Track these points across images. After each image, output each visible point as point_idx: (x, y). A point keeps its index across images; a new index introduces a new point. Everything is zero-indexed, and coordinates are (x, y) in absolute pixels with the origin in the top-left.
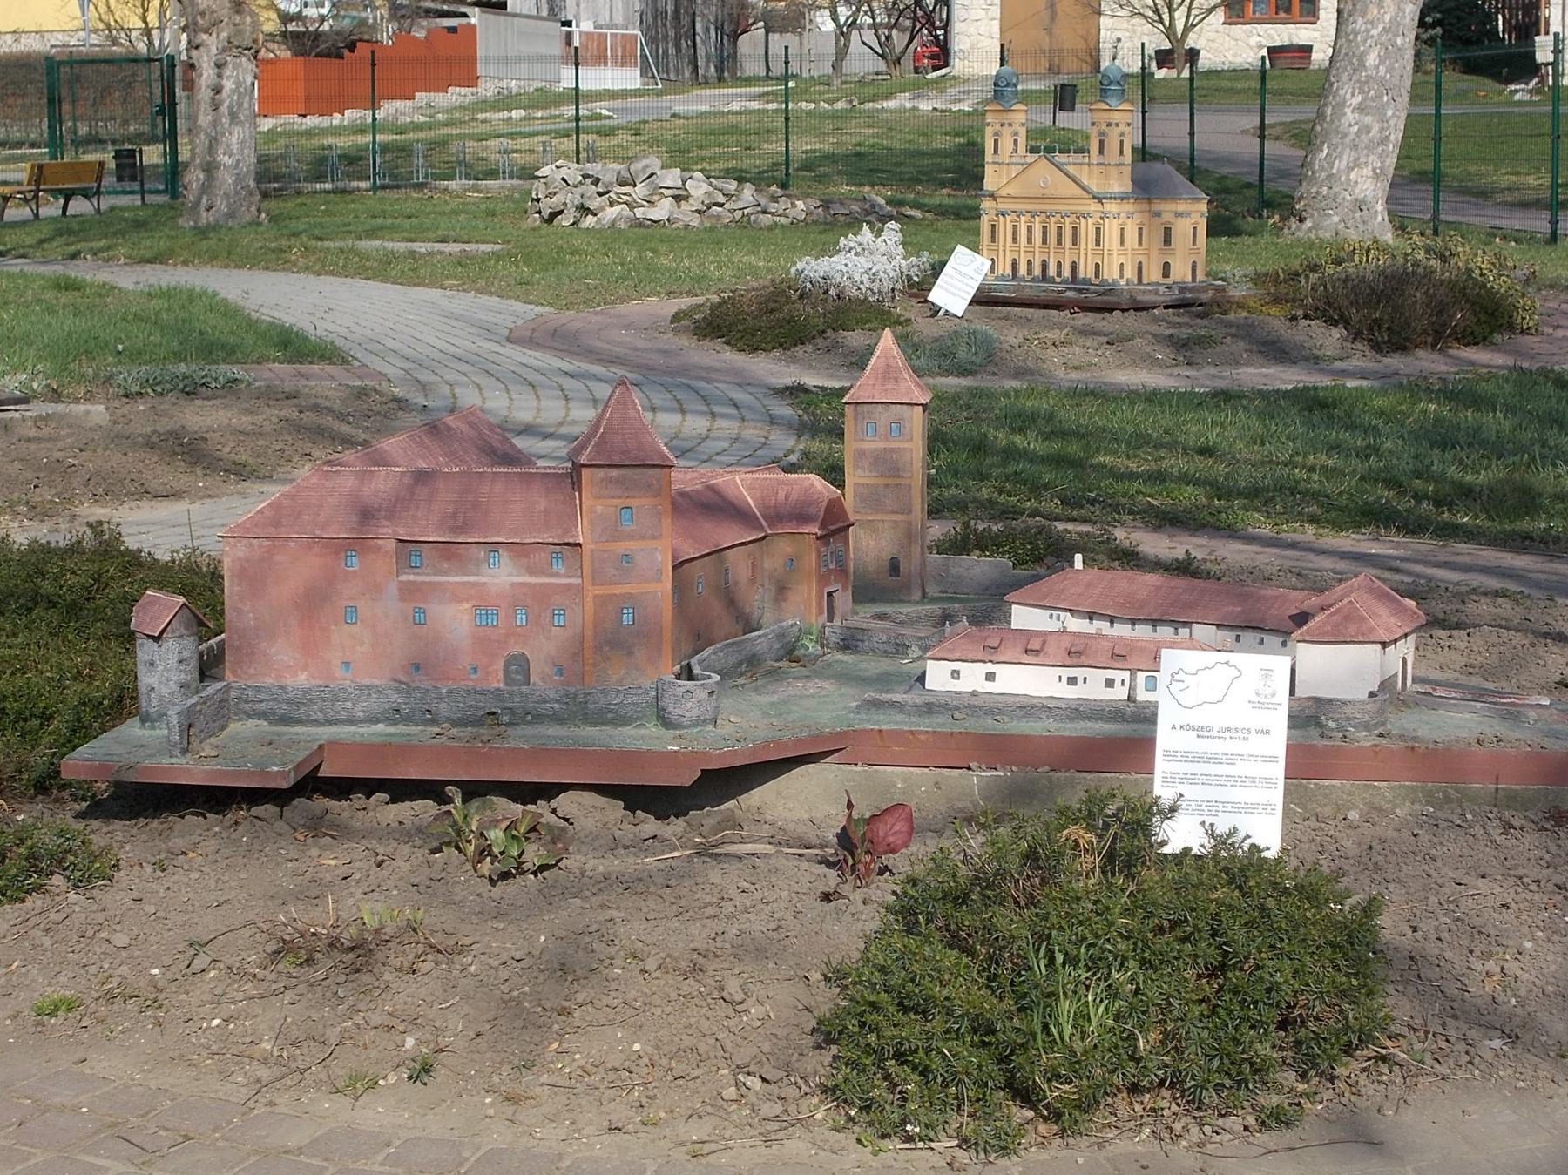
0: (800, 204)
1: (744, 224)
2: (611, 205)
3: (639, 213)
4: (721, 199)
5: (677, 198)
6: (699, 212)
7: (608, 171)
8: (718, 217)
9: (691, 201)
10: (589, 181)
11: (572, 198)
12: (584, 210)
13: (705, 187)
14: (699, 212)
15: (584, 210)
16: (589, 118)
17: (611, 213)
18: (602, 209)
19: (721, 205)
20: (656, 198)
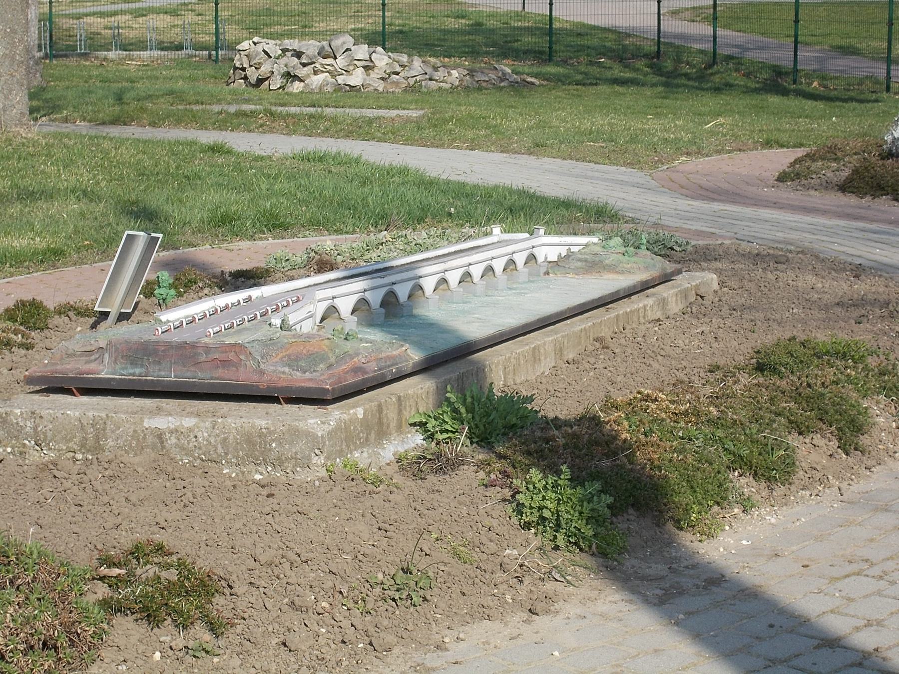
0: (455, 73)
1: (413, 89)
2: (316, 73)
3: (340, 80)
4: (398, 69)
5: (367, 68)
6: (382, 79)
7: (310, 47)
8: (397, 84)
9: (376, 70)
10: (289, 54)
11: (280, 68)
12: (290, 77)
13: (386, 60)
14: (382, 79)
15: (290, 77)
16: (391, 25)
17: (317, 80)
18: (308, 76)
19: (398, 74)
20: (351, 68)
